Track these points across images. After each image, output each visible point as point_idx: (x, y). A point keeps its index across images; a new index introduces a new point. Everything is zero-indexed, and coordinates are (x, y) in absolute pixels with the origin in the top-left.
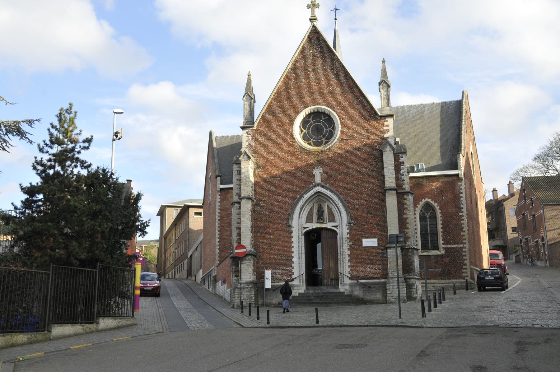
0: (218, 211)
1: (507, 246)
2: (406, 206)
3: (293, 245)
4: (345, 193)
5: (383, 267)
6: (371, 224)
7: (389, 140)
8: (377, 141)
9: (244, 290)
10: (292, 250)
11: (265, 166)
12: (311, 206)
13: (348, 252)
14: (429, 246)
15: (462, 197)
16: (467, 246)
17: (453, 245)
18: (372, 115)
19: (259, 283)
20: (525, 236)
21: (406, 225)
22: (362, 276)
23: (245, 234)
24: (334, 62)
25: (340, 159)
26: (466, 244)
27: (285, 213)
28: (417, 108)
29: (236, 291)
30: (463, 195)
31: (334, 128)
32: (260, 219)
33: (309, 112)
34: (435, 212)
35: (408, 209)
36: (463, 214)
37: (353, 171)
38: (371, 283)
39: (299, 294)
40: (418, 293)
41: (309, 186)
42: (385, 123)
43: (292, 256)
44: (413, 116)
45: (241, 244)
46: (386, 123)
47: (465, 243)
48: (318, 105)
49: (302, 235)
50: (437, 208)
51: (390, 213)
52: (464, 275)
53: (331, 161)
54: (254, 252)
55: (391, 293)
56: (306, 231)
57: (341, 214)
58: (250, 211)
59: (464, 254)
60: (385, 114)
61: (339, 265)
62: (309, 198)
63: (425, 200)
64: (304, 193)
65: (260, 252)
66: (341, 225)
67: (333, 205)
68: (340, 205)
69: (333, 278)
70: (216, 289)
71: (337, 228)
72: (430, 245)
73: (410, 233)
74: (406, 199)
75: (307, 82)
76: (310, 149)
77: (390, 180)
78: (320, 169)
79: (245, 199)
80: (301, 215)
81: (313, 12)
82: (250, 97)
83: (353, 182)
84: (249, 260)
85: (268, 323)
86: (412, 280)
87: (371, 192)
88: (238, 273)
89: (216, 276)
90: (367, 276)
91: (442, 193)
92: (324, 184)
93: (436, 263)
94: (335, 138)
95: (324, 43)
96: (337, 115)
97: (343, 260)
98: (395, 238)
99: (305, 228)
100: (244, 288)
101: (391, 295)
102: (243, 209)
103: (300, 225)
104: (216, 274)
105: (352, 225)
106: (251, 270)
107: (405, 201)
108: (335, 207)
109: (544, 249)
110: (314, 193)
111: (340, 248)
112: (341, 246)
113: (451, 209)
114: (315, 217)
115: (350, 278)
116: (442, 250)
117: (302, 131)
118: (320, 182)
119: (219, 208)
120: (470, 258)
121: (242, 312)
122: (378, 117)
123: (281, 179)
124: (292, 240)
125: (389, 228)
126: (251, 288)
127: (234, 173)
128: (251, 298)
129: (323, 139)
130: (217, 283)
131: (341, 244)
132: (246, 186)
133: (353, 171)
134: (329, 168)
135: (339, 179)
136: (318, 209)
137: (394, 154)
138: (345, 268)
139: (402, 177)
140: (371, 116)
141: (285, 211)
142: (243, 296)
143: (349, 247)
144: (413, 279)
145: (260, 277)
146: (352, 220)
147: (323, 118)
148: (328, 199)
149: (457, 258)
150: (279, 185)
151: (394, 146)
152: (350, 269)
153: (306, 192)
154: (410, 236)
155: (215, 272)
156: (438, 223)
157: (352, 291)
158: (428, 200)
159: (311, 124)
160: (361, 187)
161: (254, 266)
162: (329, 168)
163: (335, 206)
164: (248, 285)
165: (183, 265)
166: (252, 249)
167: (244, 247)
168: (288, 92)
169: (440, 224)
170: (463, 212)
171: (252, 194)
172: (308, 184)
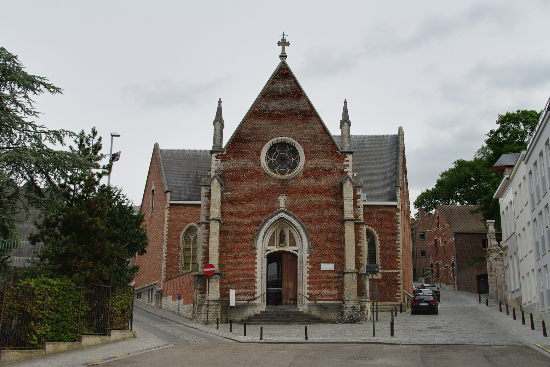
0: (166, 226)
3: (256, 266)
5: (338, 290)
8: (337, 175)
9: (211, 307)
11: (233, 190)
12: (274, 231)
13: (308, 275)
15: (399, 226)
16: (401, 271)
17: (389, 270)
18: (334, 151)
19: (223, 300)
20: (446, 264)
23: (213, 253)
24: (301, 98)
25: (303, 189)
27: (250, 235)
29: (203, 308)
31: (298, 159)
33: (276, 143)
38: (327, 304)
39: (261, 312)
40: (368, 314)
43: (256, 276)
45: (209, 263)
46: (346, 159)
47: (400, 269)
48: (285, 136)
50: (377, 235)
51: (348, 241)
52: (398, 298)
53: (295, 190)
57: (302, 240)
59: (398, 278)
61: (298, 286)
62: (273, 223)
64: (269, 218)
66: (301, 250)
67: (295, 230)
68: (302, 231)
69: (292, 298)
71: (298, 252)
74: (361, 229)
76: (276, 177)
77: (349, 213)
79: (214, 221)
80: (265, 238)
81: (283, 49)
82: (219, 120)
83: (314, 211)
84: (216, 278)
85: (261, 339)
86: (364, 303)
87: (331, 220)
88: (204, 290)
90: (324, 297)
92: (288, 210)
94: (300, 169)
95: (292, 79)
96: (302, 147)
97: (302, 282)
99: (267, 250)
100: (211, 305)
102: (212, 230)
103: (263, 248)
104: (161, 288)
105: (312, 250)
108: (296, 233)
109: (453, 274)
110: (277, 218)
111: (300, 271)
112: (301, 269)
113: (389, 237)
114: (277, 241)
115: (308, 299)
117: (268, 159)
118: (284, 208)
119: (168, 223)
120: (403, 283)
121: (218, 328)
123: (247, 203)
124: (256, 262)
125: (346, 255)
127: (202, 195)
128: (218, 314)
129: (288, 168)
130: (163, 298)
131: (301, 267)
132: (215, 208)
133: (315, 201)
134: (293, 196)
136: (280, 233)
137: (353, 187)
138: (304, 289)
139: (359, 209)
140: (332, 151)
141: (250, 234)
143: (308, 270)
144: (365, 301)
145: (224, 295)
146: (312, 246)
147: (288, 149)
148: (291, 224)
149: (393, 282)
150: (246, 209)
151: (353, 180)
152: (308, 290)
153: (271, 217)
156: (376, 249)
157: (310, 311)
158: (369, 228)
159: (277, 154)
160: (321, 216)
162: (293, 196)
163: (297, 231)
164: (215, 303)
168: (258, 122)
169: (378, 250)
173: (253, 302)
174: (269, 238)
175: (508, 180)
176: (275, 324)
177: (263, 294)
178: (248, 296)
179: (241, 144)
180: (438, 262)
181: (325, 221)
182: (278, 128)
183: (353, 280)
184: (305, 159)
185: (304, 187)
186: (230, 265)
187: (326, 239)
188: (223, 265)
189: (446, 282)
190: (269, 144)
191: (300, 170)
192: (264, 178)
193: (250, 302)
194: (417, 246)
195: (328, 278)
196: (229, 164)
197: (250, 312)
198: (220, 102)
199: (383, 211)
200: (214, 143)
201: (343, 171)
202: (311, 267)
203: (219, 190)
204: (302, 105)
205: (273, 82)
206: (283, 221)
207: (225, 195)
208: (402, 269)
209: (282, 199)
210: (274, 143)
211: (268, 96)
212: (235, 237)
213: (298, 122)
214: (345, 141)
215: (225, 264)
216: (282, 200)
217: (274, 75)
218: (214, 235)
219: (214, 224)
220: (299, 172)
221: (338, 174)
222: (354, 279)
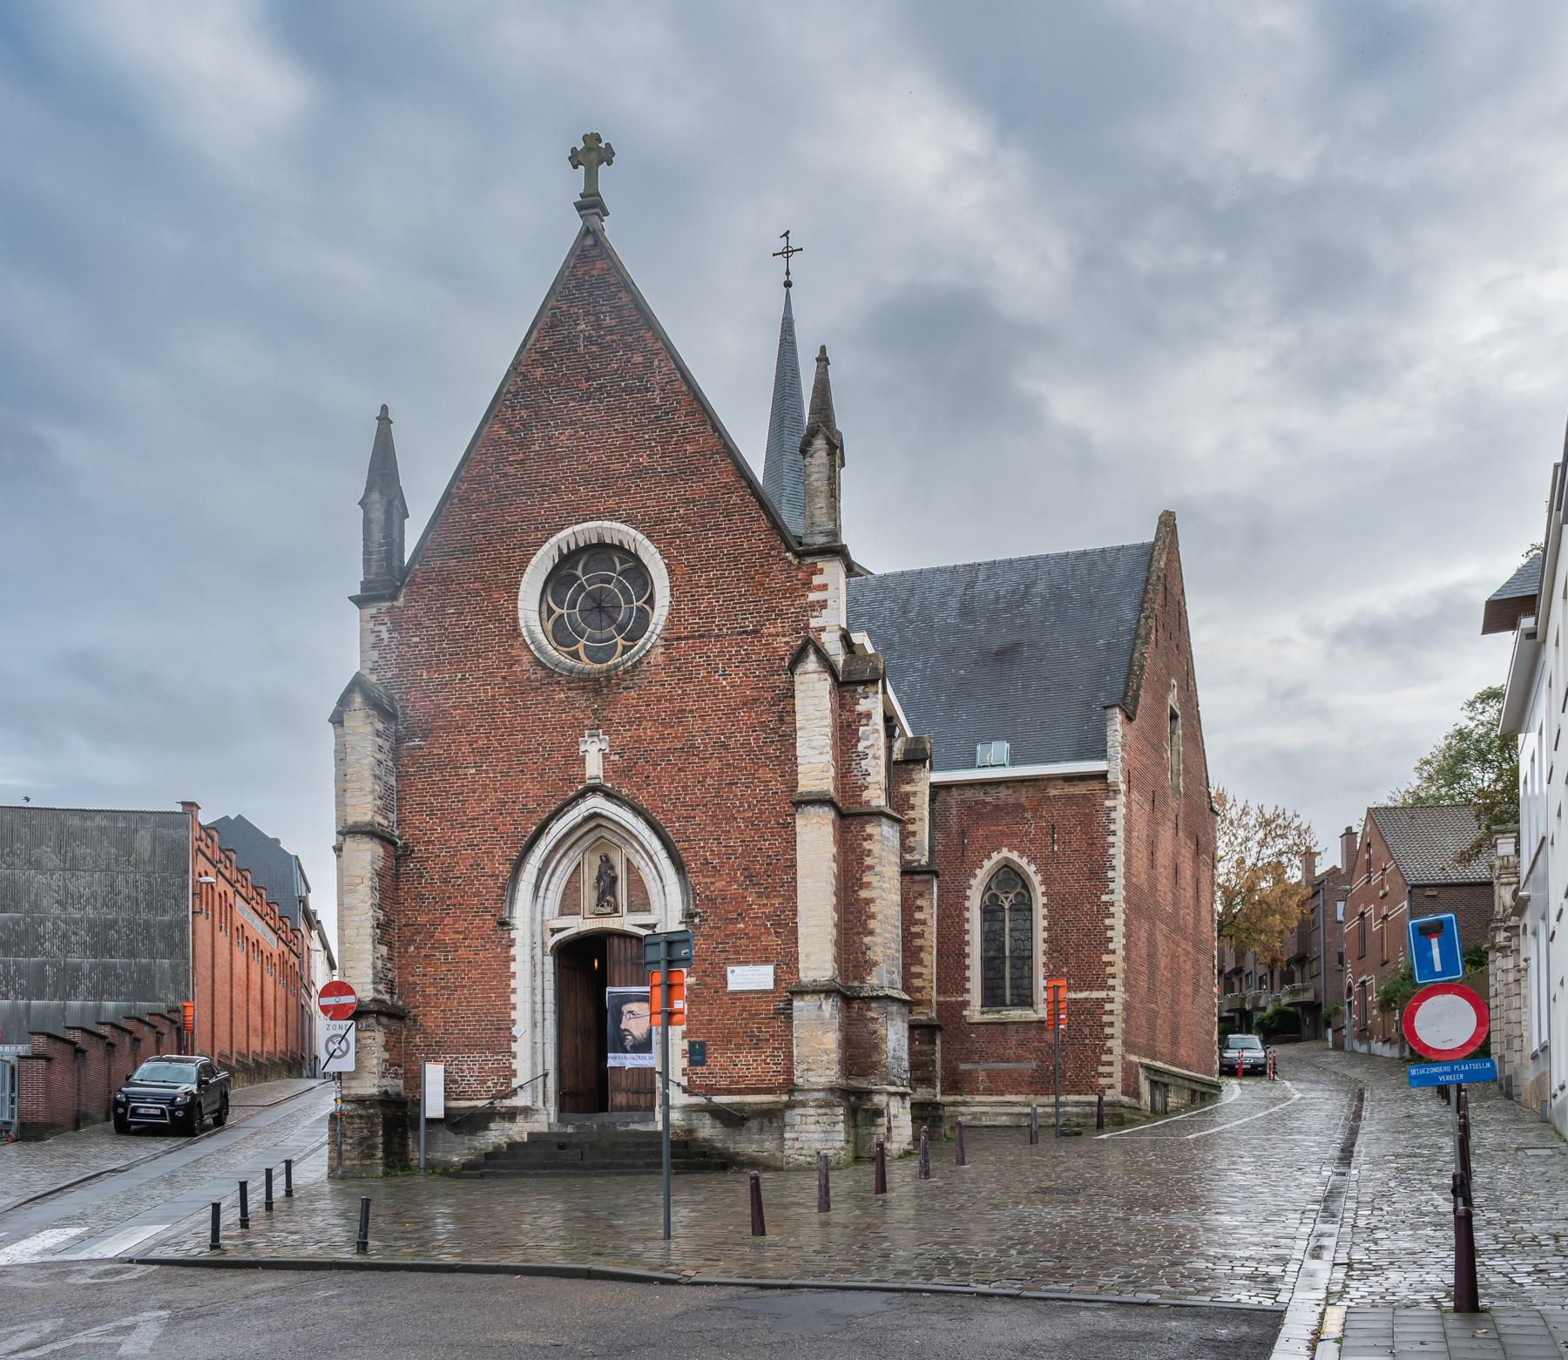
1: (1321, 1004)
2: (868, 861)
3: (513, 984)
7: (824, 637)
8: (786, 643)
14: (1004, 995)
16: (1119, 995)
17: (1075, 991)
21: (866, 920)
22: (724, 1083)
23: (357, 947)
24: (656, 363)
26: (1114, 990)
30: (1118, 840)
31: (651, 601)
33: (573, 547)
35: (878, 869)
36: (1114, 898)
46: (817, 580)
47: (1113, 988)
49: (544, 954)
50: (1036, 880)
52: (1103, 1081)
53: (637, 712)
55: (797, 1139)
59: (1105, 1019)
72: (1008, 992)
74: (870, 837)
75: (563, 437)
81: (591, 178)
83: (704, 781)
87: (761, 812)
90: (737, 1083)
93: (1021, 1044)
98: (663, 946)
99: (554, 931)
101: (797, 1145)
107: (867, 845)
110: (580, 819)
113: (1078, 881)
114: (588, 895)
115: (685, 1090)
117: (550, 611)
123: (479, 772)
129: (619, 639)
135: (661, 772)
139: (863, 762)
141: (491, 876)
146: (697, 906)
149: (1087, 1031)
154: (879, 958)
158: (1010, 855)
160: (728, 798)
163: (647, 859)
164: (365, 1108)
168: (506, 475)
172: (563, 787)
173: (507, 1103)
175: (1531, 641)
176: (550, 1175)
177: (540, 1072)
178: (489, 1084)
179: (453, 563)
180: (1364, 977)
182: (574, 492)
184: (672, 595)
189: (1384, 1036)
190: (545, 553)
191: (655, 637)
192: (533, 677)
193: (497, 1103)
194: (1328, 940)
195: (753, 1016)
198: (384, 419)
199: (1060, 797)
200: (367, 571)
201: (807, 627)
204: (657, 392)
205: (554, 315)
207: (409, 748)
210: (565, 551)
211: (539, 372)
213: (644, 460)
214: (817, 512)
217: (560, 288)
222: (827, 1015)
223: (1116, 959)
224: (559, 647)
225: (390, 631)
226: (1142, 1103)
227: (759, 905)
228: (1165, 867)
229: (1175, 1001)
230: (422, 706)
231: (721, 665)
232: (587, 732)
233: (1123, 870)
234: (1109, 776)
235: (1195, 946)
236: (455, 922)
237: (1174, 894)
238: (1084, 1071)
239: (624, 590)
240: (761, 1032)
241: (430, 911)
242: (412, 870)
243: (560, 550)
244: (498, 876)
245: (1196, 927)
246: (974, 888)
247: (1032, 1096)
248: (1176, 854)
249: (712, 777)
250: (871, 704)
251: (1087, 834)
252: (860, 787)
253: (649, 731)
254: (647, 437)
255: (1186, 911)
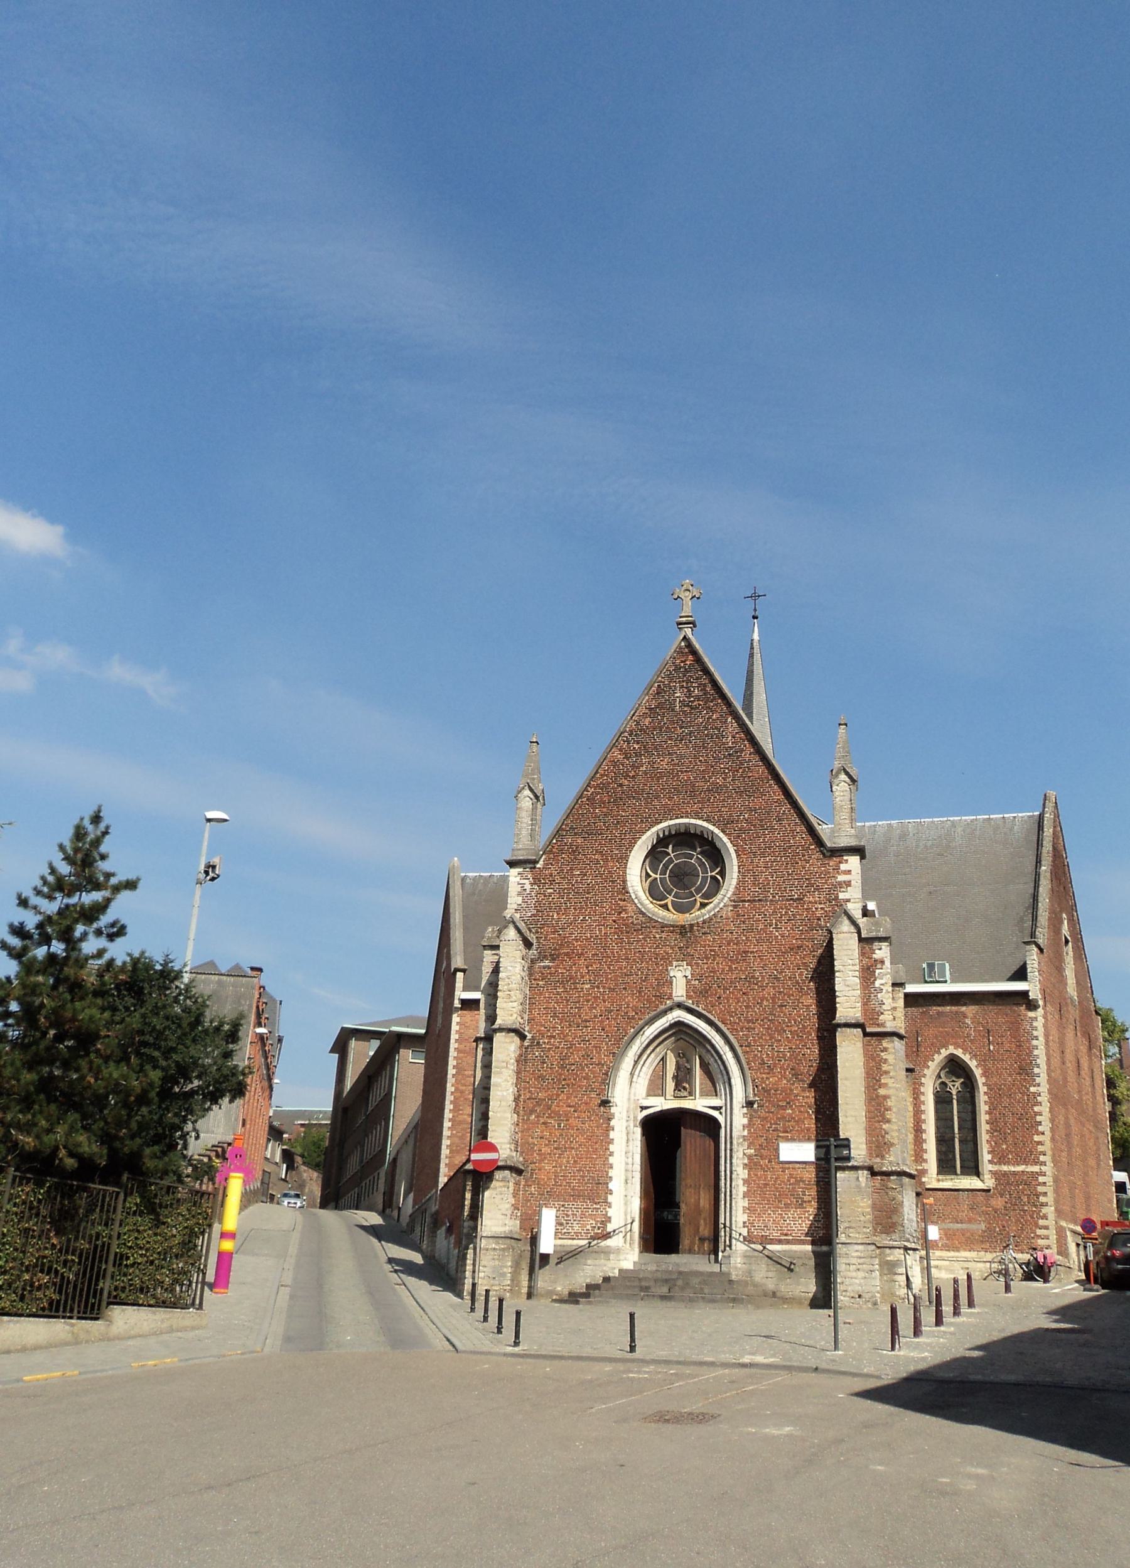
3: (612, 1148)
4: (742, 1029)
6: (802, 1106)
8: (821, 908)
10: (610, 1162)
12: (661, 1056)
16: (1048, 1169)
21: (884, 1112)
22: (776, 1235)
24: (729, 720)
28: (937, 828)
30: (1040, 1043)
31: (722, 873)
32: (539, 1083)
34: (971, 1082)
36: (1040, 1089)
37: (763, 977)
41: (657, 1006)
42: (841, 865)
43: (610, 1175)
44: (926, 846)
46: (843, 867)
47: (1044, 1163)
49: (635, 1126)
53: (711, 951)
54: (520, 1162)
56: (646, 1116)
58: (512, 1061)
59: (1040, 1189)
60: (842, 845)
63: (948, 1052)
65: (535, 1163)
67: (712, 1056)
70: (435, 1246)
71: (721, 1113)
73: (895, 1134)
74: (885, 1050)
75: (664, 764)
78: (685, 967)
80: (635, 1077)
89: (437, 1213)
90: (786, 1235)
91: (989, 1036)
92: (693, 1004)
99: (643, 1108)
100: (487, 1250)
103: (632, 1101)
106: (508, 1206)
108: (716, 1061)
110: (668, 1024)
113: (1010, 1075)
114: (670, 1085)
116: (987, 1176)
117: (648, 875)
118: (684, 999)
120: (1057, 1201)
122: (825, 851)
126: (503, 1250)
127: (483, 968)
128: (503, 1275)
132: (507, 1000)
133: (763, 977)
137: (861, 939)
139: (879, 995)
142: (485, 1269)
143: (746, 1161)
146: (755, 1095)
148: (701, 1040)
150: (588, 1001)
151: (862, 922)
152: (746, 1215)
154: (895, 1141)
155: (435, 1205)
156: (977, 1109)
157: (749, 1273)
158: (955, 1052)
159: (671, 861)
160: (779, 1016)
161: (515, 1195)
162: (706, 966)
163: (717, 1058)
165: (378, 1179)
166: (514, 1154)
167: (492, 1148)
168: (621, 785)
170: (1039, 1085)
171: (522, 1021)
173: (604, 1243)
174: (649, 1077)
177: (630, 1221)
178: (589, 1227)
181: (789, 1029)
182: (670, 799)
183: (859, 1187)
184: (739, 872)
185: (737, 944)
186: (546, 1145)
187: (791, 1079)
188: (529, 1145)
192: (635, 922)
195: (798, 1182)
196: (552, 891)
197: (589, 1272)
201: (836, 898)
202: (753, 1151)
203: (519, 954)
204: (730, 738)
206: (683, 1031)
207: (540, 967)
208: (1050, 1164)
209: (679, 975)
211: (647, 721)
212: (561, 1075)
215: (534, 1144)
216: (680, 978)
218: (503, 1068)
219: (503, 1039)
220: (722, 905)
221: (822, 906)
222: (863, 1185)
223: (1044, 1137)
224: (654, 901)
225: (532, 884)
226: (1072, 1262)
227: (803, 1097)
228: (1071, 1062)
229: (1086, 1174)
230: (552, 938)
231: (774, 921)
232: (674, 963)
233: (1046, 1068)
234: (1030, 994)
235: (1096, 1126)
236: (568, 1098)
237: (1078, 1083)
238: (1025, 1233)
239: (702, 864)
240: (805, 1195)
241: (549, 1089)
242: (537, 1057)
243: (658, 835)
244: (603, 1065)
245: (1094, 1110)
246: (927, 1077)
247: (983, 1253)
248: (1077, 1051)
249: (767, 1000)
250: (882, 952)
251: (1015, 1038)
252: (878, 1013)
253: (721, 965)
254: (722, 766)
255: (1088, 1097)
